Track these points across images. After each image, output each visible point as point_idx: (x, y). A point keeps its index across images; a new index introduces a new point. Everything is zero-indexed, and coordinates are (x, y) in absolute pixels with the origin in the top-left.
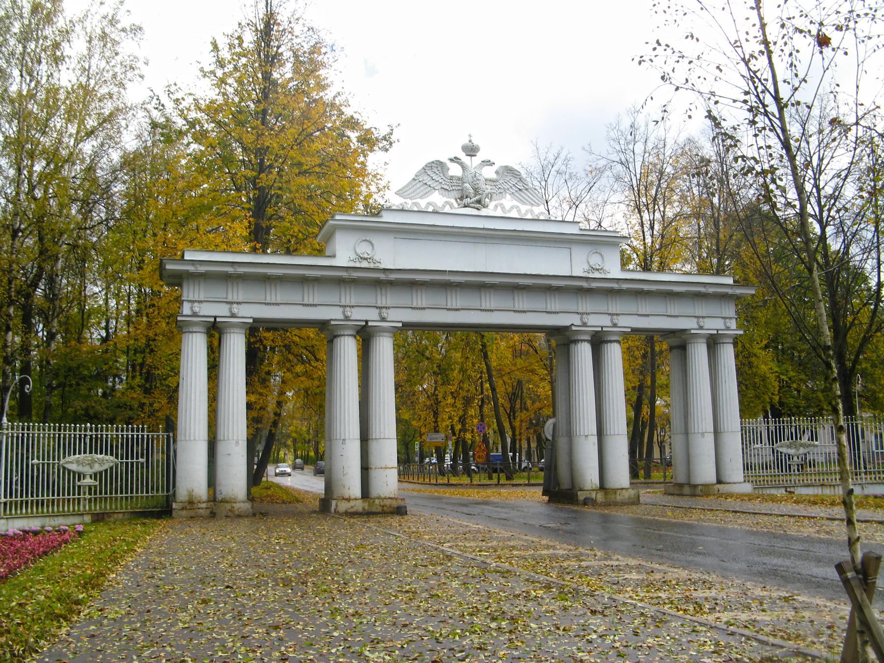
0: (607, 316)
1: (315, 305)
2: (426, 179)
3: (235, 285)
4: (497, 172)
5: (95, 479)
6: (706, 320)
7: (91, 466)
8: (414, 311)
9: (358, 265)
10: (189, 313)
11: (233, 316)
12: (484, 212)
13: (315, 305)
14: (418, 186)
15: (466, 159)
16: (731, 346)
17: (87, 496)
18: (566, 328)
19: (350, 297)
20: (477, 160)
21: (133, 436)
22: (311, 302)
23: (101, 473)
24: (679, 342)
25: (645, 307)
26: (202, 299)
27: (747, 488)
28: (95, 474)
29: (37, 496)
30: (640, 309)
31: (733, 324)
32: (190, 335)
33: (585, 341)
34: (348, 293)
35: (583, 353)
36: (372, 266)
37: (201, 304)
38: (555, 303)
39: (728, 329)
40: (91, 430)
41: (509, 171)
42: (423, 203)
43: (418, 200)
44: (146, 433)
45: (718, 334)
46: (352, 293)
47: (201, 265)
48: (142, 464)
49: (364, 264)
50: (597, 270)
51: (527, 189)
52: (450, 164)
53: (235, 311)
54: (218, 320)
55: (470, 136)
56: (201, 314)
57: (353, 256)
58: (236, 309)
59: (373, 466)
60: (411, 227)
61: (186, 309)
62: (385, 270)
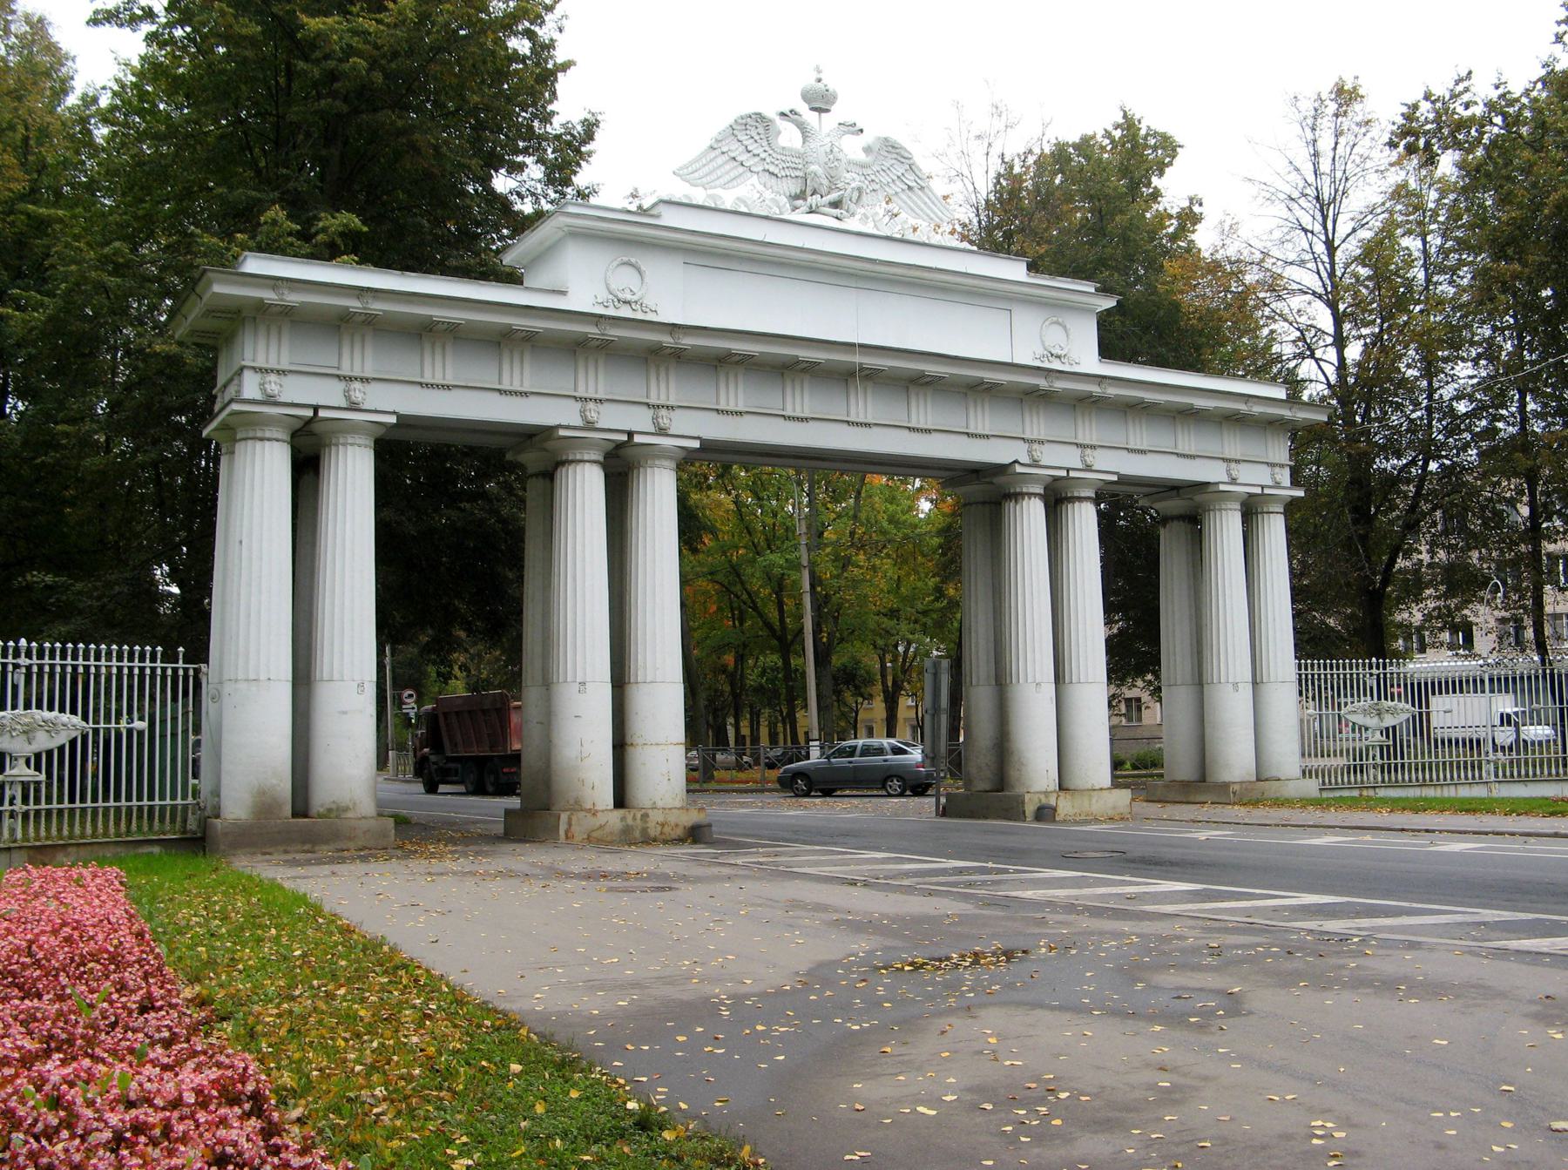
0: (645, 408)
1: (525, 394)
2: (736, 149)
3: (357, 338)
4: (867, 150)
5: (38, 768)
6: (1243, 466)
7: (28, 733)
8: (721, 418)
9: (611, 312)
10: (258, 396)
11: (354, 407)
12: (852, 224)
13: (525, 394)
14: (720, 161)
15: (810, 117)
16: (1282, 517)
17: (19, 807)
18: (1001, 469)
19: (595, 381)
20: (829, 121)
21: (120, 669)
22: (516, 387)
23: (50, 753)
24: (1189, 507)
25: (1140, 435)
26: (285, 366)
27: (1311, 787)
28: (38, 756)
29: (140, 798)
30: (1271, 454)
31: (1285, 477)
32: (259, 444)
33: (1035, 495)
34: (438, 358)
35: (1030, 518)
36: (640, 316)
37: (271, 378)
38: (983, 419)
39: (1277, 485)
40: (29, 655)
41: (891, 149)
42: (728, 200)
43: (719, 191)
44: (158, 664)
45: (1067, 478)
46: (527, 366)
47: (291, 290)
48: (141, 733)
49: (625, 312)
50: (1059, 357)
51: (922, 188)
52: (782, 124)
53: (357, 396)
54: (322, 414)
55: (957, 105)
56: (282, 400)
57: (603, 295)
58: (358, 392)
59: (639, 741)
60: (926, 275)
61: (251, 387)
62: (673, 328)
